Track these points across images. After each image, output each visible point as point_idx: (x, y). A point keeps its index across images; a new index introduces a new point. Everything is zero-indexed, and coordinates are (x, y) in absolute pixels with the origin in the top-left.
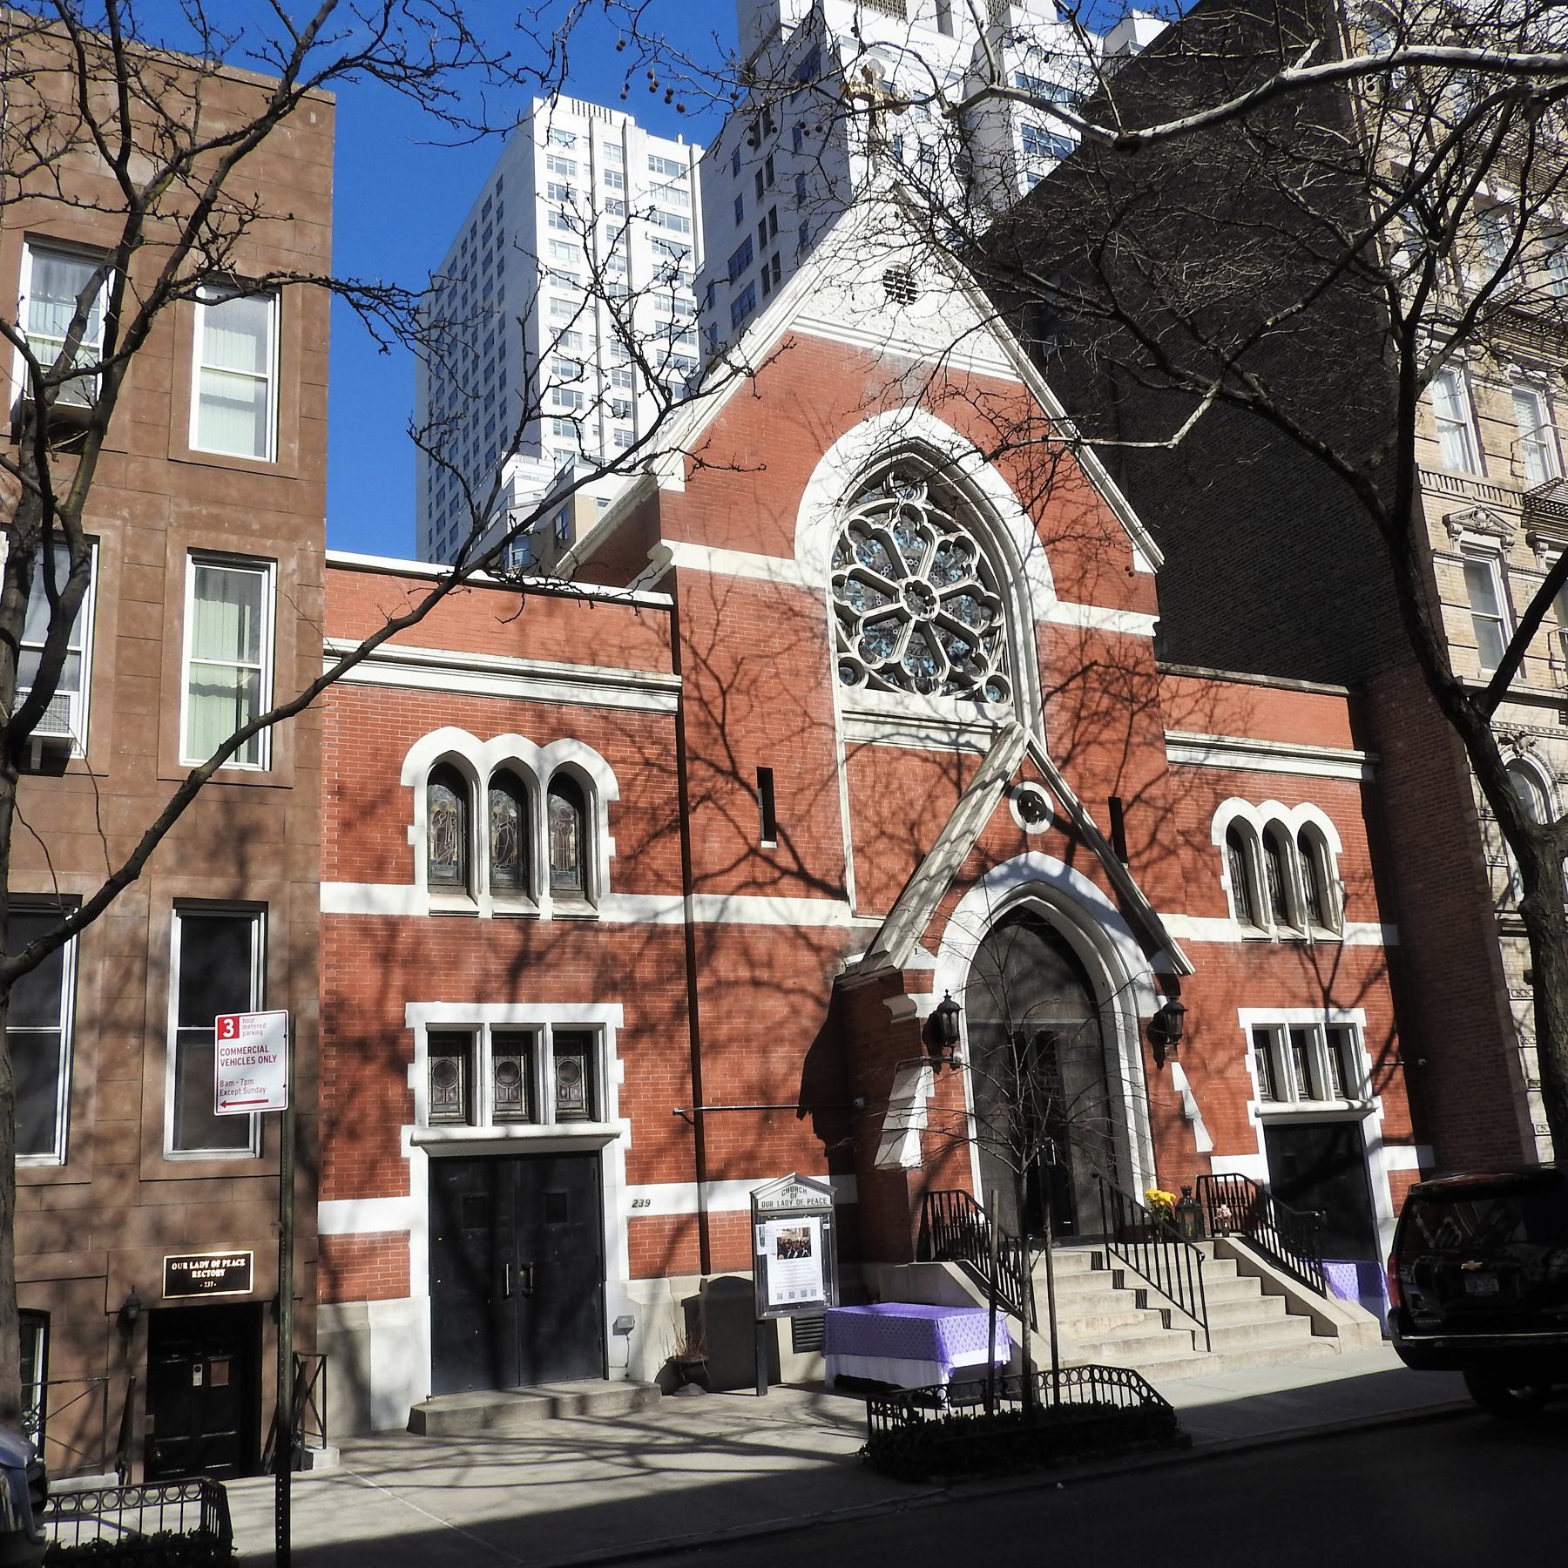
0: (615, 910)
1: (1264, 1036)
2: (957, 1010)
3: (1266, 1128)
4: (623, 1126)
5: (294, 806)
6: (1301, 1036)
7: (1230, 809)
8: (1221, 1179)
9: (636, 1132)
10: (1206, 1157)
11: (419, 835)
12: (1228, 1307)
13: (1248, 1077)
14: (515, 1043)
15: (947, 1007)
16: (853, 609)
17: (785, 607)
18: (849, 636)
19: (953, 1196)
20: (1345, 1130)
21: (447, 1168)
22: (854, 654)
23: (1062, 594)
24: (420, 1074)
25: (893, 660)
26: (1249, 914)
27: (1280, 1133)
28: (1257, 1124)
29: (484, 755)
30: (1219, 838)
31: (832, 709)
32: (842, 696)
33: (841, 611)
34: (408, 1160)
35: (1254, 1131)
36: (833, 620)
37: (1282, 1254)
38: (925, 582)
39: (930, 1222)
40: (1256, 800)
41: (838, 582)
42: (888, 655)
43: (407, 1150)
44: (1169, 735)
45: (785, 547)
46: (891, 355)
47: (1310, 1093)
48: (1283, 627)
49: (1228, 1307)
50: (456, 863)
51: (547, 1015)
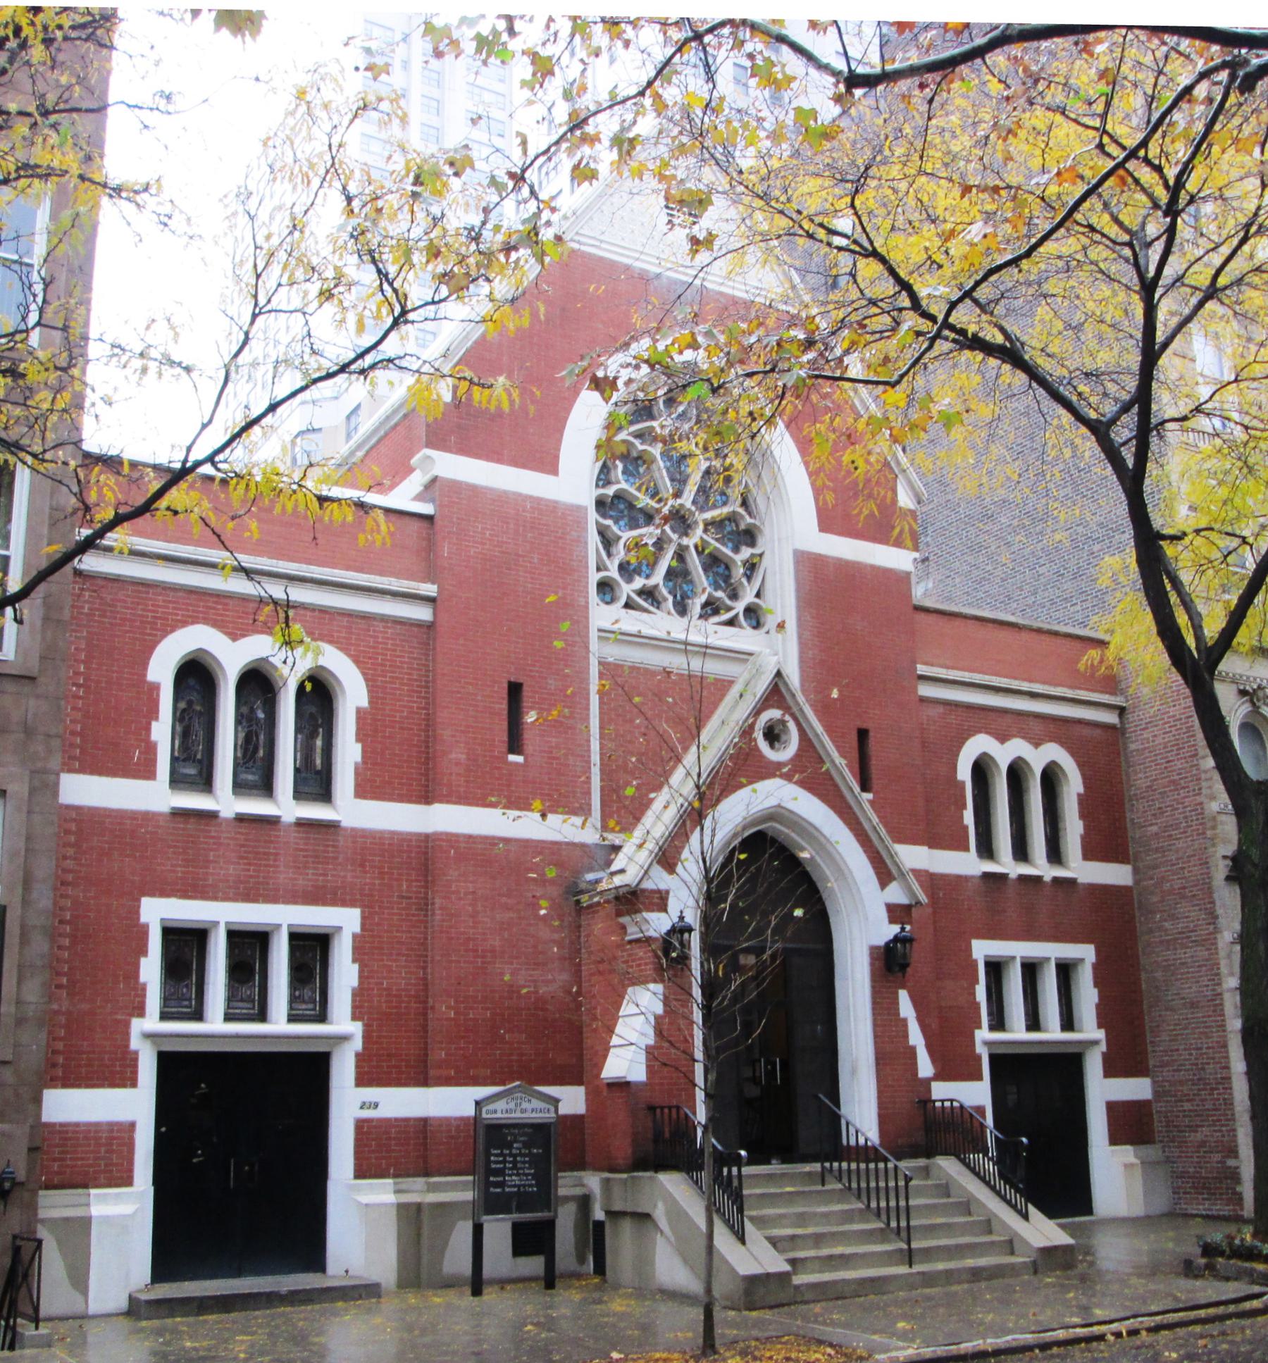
0: (351, 810)
1: (996, 969)
2: (690, 930)
3: (993, 1058)
4: (355, 1029)
5: (38, 697)
6: (1031, 970)
7: (978, 745)
8: (938, 1104)
9: (367, 1037)
10: (927, 1082)
11: (162, 731)
12: (931, 1230)
13: (977, 1006)
14: (249, 948)
15: (681, 930)
16: (615, 528)
17: (549, 522)
18: (609, 555)
19: (666, 1110)
20: (1064, 1068)
21: (177, 1068)
22: (613, 573)
23: (777, 814)
24: (151, 969)
25: (651, 582)
26: (986, 849)
27: (1008, 1067)
28: (983, 1052)
29: (233, 656)
30: (964, 772)
31: (587, 627)
32: (602, 615)
33: (603, 532)
34: (136, 1053)
35: (979, 1058)
36: (593, 539)
37: (1000, 1184)
38: (688, 505)
39: (451, 1102)
40: (1003, 738)
41: (601, 504)
42: (648, 577)
43: (135, 1043)
44: (922, 669)
45: (549, 464)
46: (668, 278)
47: (1034, 1023)
48: (1041, 570)
49: (931, 1230)
50: (200, 762)
51: (283, 917)
